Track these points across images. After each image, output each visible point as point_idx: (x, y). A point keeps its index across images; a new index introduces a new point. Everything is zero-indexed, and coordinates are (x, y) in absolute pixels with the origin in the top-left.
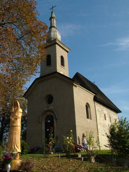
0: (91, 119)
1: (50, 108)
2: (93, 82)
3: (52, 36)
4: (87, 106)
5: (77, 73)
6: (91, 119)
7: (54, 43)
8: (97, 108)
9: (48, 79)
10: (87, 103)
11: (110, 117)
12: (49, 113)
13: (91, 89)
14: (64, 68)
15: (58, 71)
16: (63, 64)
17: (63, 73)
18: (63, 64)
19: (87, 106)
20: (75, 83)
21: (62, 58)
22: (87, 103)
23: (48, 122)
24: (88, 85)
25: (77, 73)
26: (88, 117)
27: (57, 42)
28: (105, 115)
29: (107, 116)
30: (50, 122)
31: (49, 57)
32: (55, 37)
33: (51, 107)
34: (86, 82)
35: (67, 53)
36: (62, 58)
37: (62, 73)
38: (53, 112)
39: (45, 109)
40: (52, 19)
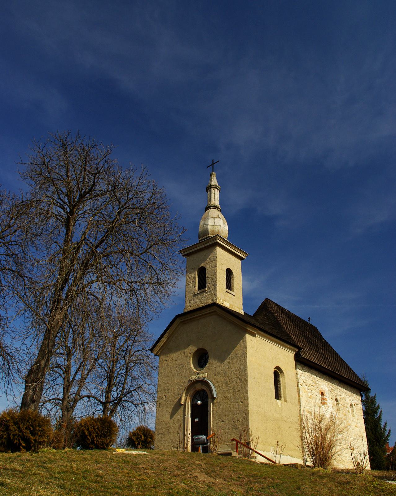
0: (286, 401)
1: (201, 376)
2: (307, 320)
3: (210, 228)
4: (277, 373)
5: (267, 300)
6: (286, 401)
7: (213, 244)
8: (303, 378)
9: (200, 316)
10: (278, 368)
11: (337, 400)
12: (199, 387)
13: (293, 337)
14: (233, 293)
15: (219, 302)
16: (229, 285)
17: (230, 305)
18: (229, 285)
19: (277, 373)
20: (249, 327)
21: (229, 273)
22: (278, 368)
23: (197, 404)
24: (288, 327)
25: (267, 300)
26: (278, 397)
27: (218, 241)
28: (322, 394)
29: (327, 396)
30: (201, 405)
31: (202, 272)
32: (216, 229)
33: (204, 375)
34: (282, 319)
35: (240, 261)
36: (229, 273)
37: (227, 305)
38: (207, 384)
39: (193, 378)
40: (210, 191)
